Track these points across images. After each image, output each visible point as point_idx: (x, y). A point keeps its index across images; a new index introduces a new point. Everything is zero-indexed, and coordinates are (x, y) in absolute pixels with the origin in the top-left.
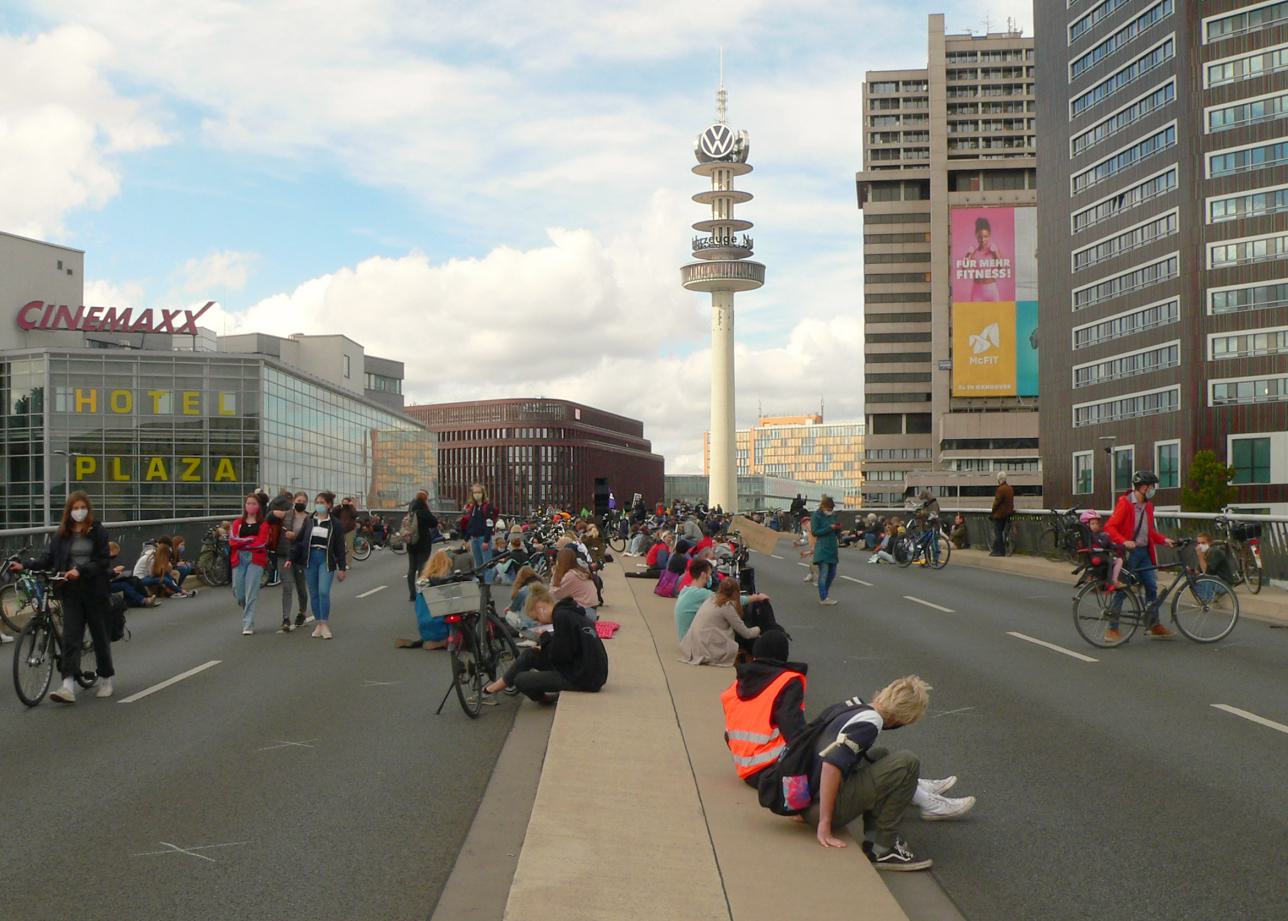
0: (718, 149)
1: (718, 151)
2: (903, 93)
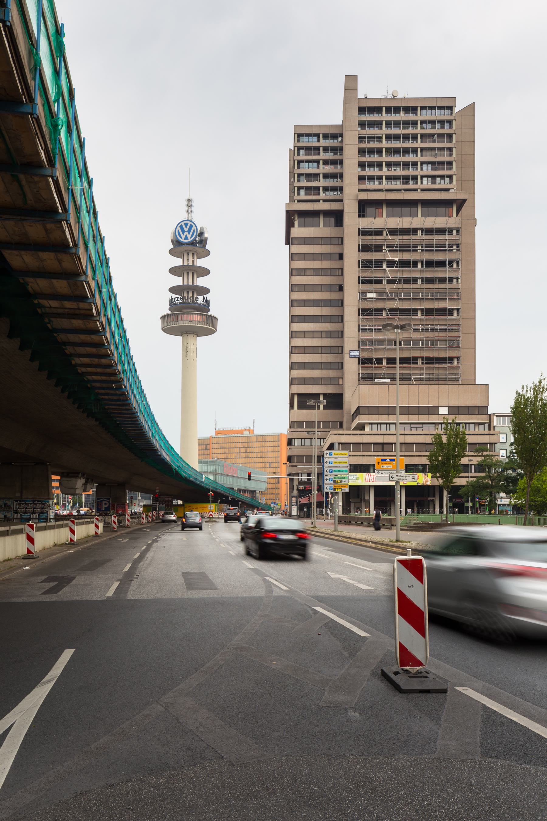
1: (186, 238)
2: (323, 143)
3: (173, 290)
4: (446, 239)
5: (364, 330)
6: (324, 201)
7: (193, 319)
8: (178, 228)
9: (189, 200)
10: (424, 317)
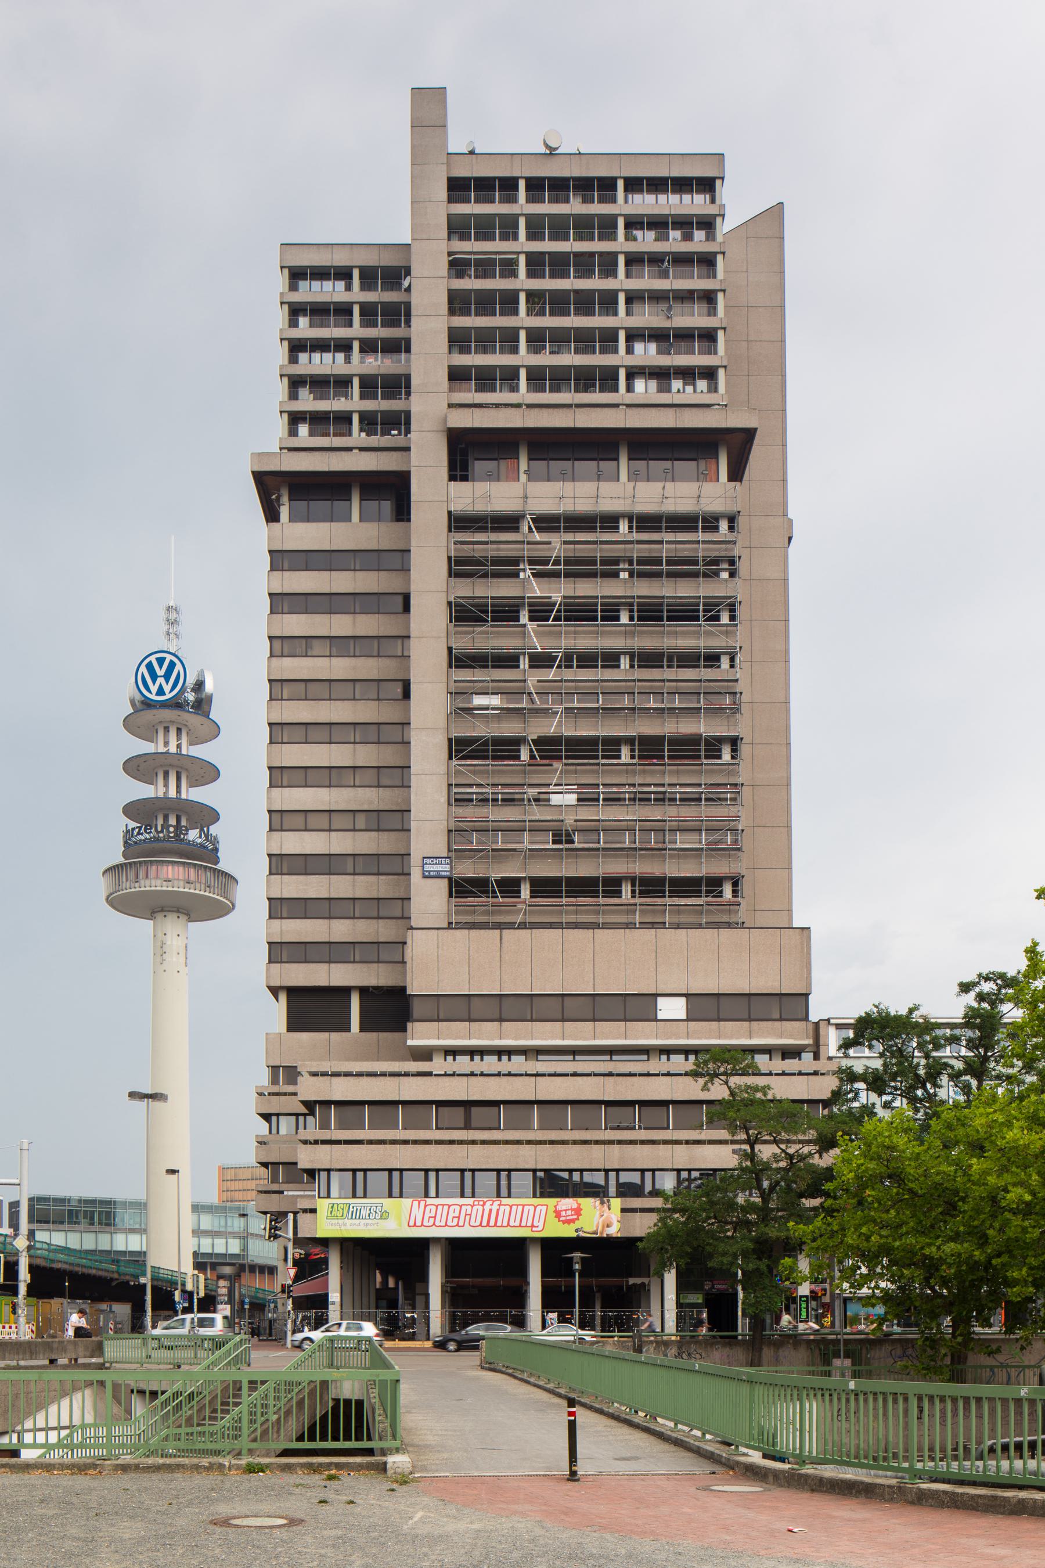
0: (161, 688)
1: (161, 691)
3: (131, 810)
4: (697, 544)
5: (462, 801)
7: (171, 878)
8: (143, 669)
10: (634, 761)
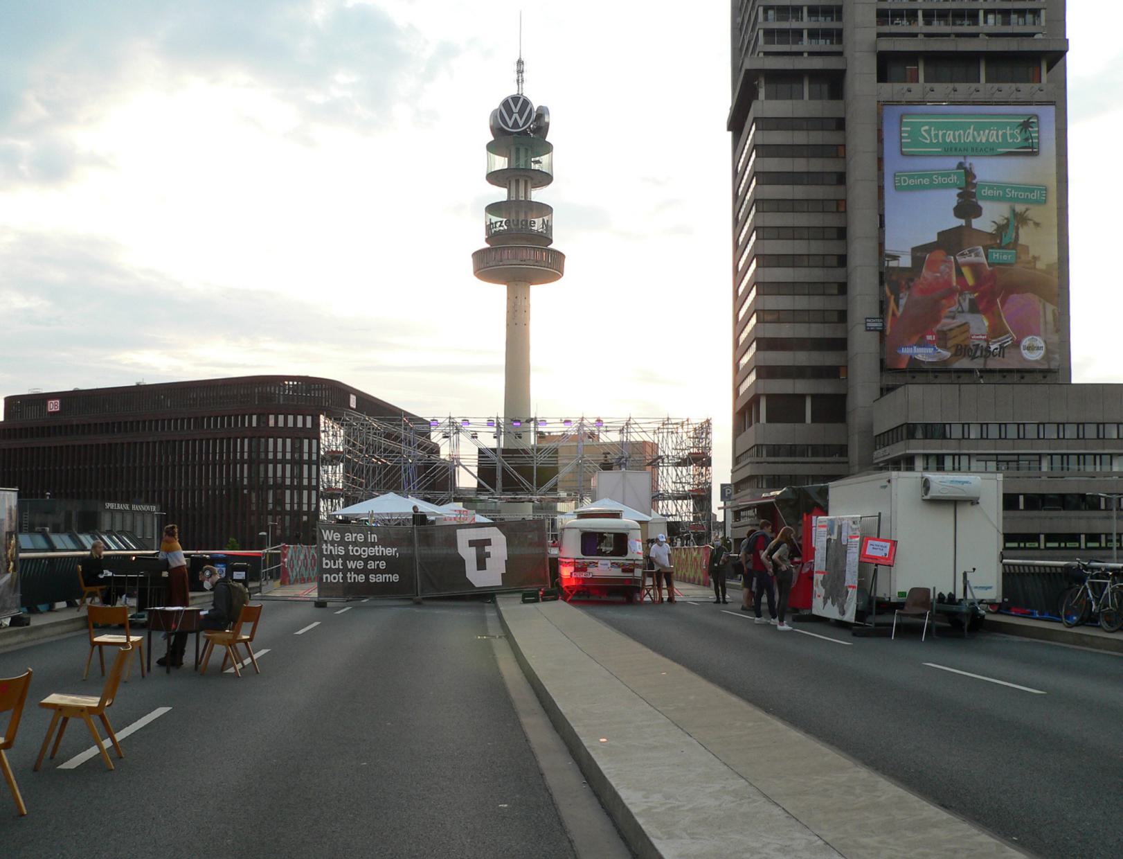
1: (516, 124)
3: (493, 209)
6: (811, 54)
9: (520, 63)
